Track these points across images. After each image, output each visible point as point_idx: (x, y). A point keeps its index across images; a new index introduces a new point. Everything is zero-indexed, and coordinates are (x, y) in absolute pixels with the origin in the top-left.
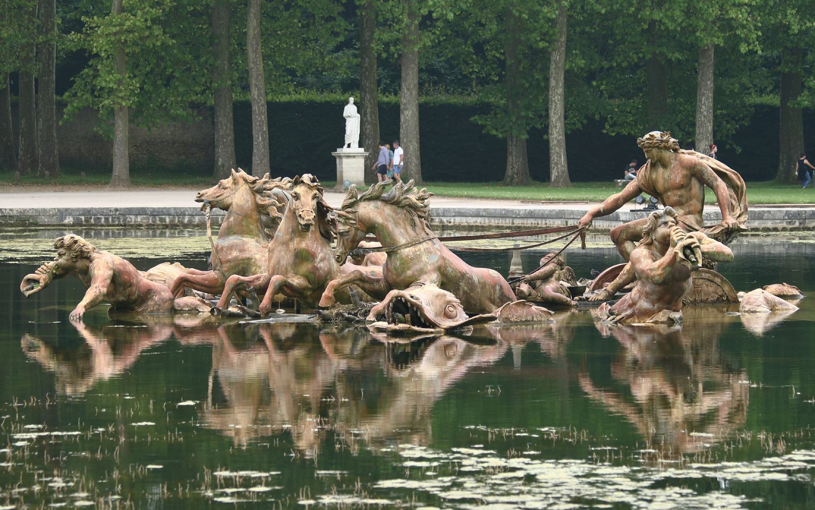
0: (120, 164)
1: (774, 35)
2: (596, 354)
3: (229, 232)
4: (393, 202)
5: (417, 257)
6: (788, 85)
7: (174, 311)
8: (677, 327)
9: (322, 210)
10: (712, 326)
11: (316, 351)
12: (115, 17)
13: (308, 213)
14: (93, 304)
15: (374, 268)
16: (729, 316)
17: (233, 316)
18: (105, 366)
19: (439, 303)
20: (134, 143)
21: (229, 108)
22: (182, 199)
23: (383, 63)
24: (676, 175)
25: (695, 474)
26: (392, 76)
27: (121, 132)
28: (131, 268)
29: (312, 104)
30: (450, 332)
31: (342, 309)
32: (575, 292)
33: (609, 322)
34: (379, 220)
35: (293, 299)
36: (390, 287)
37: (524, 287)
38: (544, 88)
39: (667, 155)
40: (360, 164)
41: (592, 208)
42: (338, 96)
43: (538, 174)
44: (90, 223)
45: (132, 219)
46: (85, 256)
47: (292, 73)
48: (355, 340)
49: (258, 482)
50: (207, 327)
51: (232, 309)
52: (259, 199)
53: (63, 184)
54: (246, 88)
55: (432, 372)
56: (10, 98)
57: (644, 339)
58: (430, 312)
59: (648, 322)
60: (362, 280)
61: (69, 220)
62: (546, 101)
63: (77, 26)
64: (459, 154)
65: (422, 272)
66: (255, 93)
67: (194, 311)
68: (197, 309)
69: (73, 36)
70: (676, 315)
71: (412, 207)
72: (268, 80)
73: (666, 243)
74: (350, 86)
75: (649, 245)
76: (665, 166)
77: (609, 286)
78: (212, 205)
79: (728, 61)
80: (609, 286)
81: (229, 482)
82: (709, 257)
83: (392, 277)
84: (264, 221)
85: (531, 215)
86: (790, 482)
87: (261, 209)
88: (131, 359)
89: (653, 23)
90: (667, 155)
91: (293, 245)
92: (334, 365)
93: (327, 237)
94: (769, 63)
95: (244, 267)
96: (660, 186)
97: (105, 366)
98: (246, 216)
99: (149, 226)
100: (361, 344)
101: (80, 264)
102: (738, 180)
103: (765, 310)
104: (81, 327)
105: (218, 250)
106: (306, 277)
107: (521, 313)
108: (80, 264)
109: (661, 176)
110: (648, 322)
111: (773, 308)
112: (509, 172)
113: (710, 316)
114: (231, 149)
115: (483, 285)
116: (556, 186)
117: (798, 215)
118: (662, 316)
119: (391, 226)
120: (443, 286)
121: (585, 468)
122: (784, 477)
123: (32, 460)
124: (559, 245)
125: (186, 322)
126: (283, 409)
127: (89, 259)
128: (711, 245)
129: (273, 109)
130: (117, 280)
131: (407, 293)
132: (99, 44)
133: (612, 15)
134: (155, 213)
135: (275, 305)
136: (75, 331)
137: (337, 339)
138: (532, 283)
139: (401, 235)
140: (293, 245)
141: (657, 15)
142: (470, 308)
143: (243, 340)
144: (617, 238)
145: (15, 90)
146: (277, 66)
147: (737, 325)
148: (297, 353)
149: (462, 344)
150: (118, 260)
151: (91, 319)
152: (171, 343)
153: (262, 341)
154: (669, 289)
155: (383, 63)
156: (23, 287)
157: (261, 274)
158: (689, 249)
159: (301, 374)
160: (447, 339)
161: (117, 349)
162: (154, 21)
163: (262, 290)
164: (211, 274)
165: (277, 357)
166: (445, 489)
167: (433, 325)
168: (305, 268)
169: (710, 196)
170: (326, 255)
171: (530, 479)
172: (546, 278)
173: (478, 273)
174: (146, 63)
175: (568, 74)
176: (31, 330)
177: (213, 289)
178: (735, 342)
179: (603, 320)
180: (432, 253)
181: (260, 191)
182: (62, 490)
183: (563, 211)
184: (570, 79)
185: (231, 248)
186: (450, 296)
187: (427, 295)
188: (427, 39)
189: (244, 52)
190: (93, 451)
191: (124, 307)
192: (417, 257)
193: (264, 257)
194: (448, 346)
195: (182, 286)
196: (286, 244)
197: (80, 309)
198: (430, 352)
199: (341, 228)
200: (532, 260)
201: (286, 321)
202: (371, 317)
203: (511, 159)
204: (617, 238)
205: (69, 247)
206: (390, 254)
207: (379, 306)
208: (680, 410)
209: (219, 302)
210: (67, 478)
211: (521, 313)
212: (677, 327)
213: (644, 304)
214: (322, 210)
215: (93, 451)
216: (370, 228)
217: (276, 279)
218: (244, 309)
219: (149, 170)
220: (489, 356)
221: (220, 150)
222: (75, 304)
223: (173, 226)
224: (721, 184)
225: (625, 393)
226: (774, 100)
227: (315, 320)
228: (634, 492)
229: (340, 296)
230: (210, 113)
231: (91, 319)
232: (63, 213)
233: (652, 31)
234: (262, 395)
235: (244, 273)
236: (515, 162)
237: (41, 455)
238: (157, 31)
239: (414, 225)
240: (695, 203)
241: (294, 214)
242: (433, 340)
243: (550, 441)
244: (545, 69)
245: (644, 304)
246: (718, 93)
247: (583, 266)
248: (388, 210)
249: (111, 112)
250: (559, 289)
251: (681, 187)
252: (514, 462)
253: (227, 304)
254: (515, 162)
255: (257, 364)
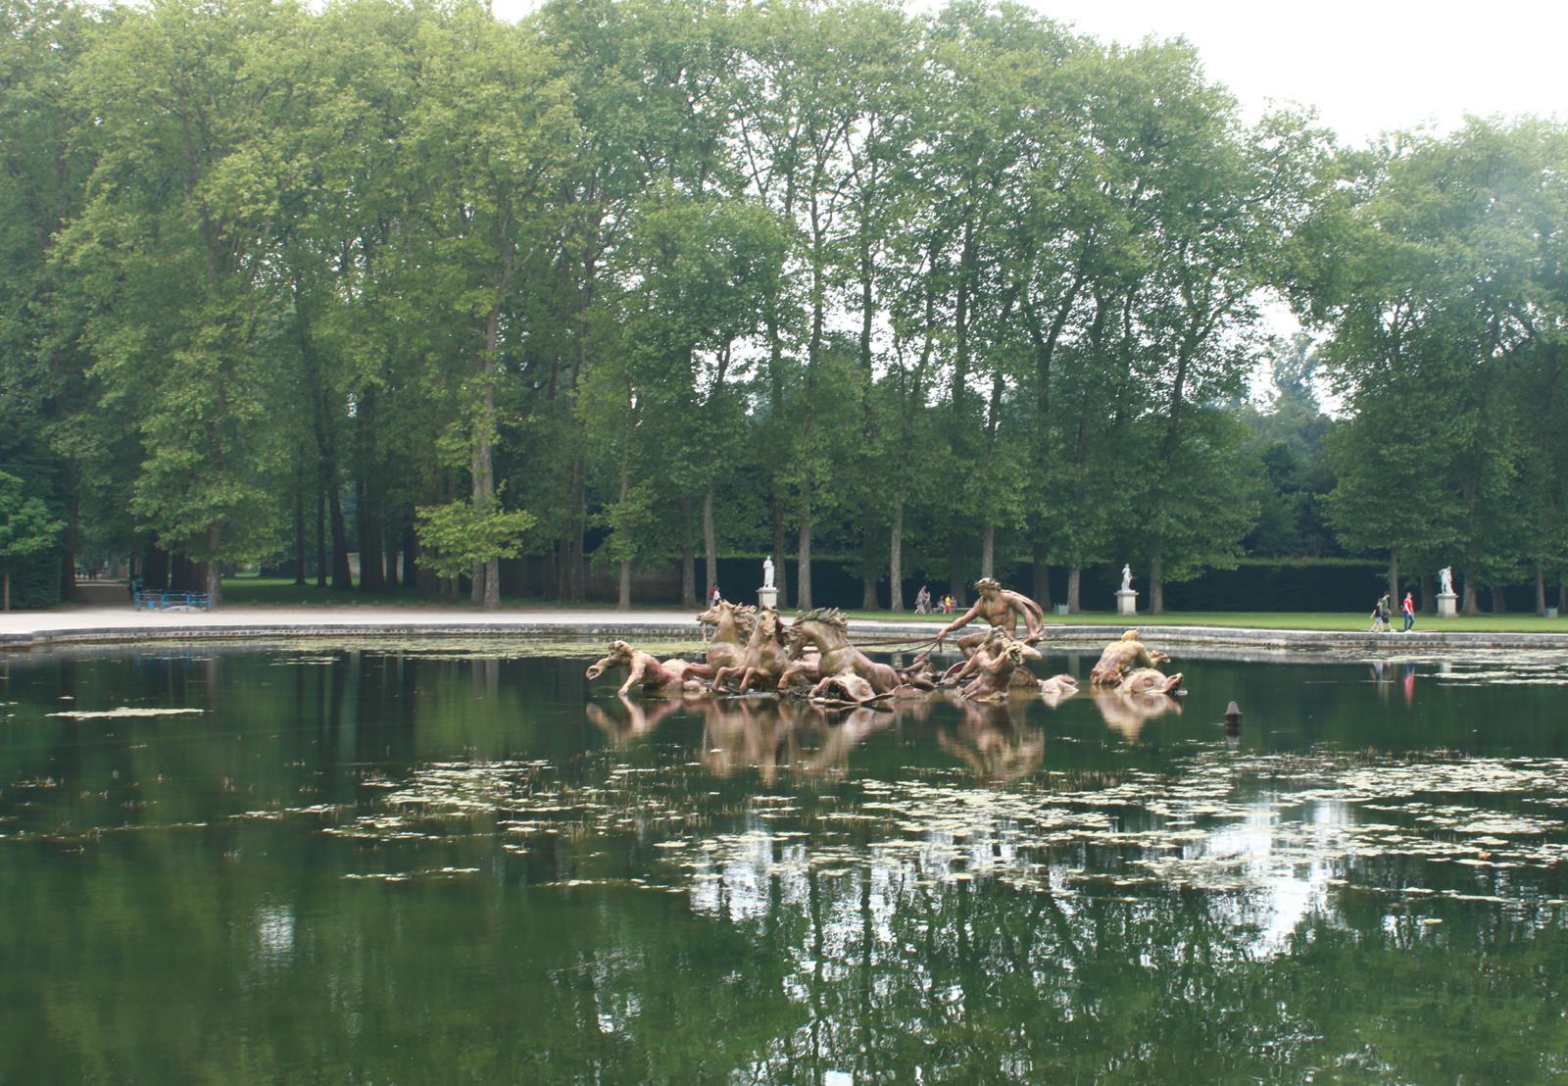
0: (624, 597)
1: (1033, 518)
2: (947, 716)
3: (718, 640)
4: (822, 621)
5: (840, 657)
6: (1040, 551)
7: (684, 690)
8: (1006, 702)
9: (779, 626)
10: (1023, 702)
11: (775, 715)
12: (622, 504)
13: (770, 629)
14: (633, 685)
15: (813, 661)
16: (1033, 696)
17: (722, 693)
18: (640, 723)
19: (857, 686)
20: (633, 584)
21: (692, 562)
22: (688, 620)
23: (788, 535)
24: (1000, 607)
25: (1066, 800)
26: (793, 543)
27: (625, 576)
28: (656, 662)
29: (743, 560)
30: (865, 704)
31: (792, 689)
32: (935, 679)
33: (963, 699)
34: (817, 633)
35: (759, 682)
36: (823, 675)
37: (904, 676)
38: (888, 552)
39: (994, 593)
40: (1453, 603)
41: (944, 627)
42: (758, 555)
43: (883, 604)
44: (629, 633)
45: (635, 631)
46: (627, 655)
47: (732, 540)
48: (801, 710)
49: (784, 804)
50: (705, 700)
51: (721, 689)
52: (737, 620)
53: (402, 606)
54: (703, 550)
55: (852, 729)
56: (554, 555)
57: (985, 709)
58: (852, 692)
59: (987, 699)
60: (805, 671)
61: (595, 631)
62: (890, 559)
63: (599, 510)
64: (840, 588)
65: (843, 666)
66: (708, 553)
67: (696, 690)
68: (698, 688)
69: (595, 516)
70: (1005, 695)
71: (837, 625)
72: (717, 544)
73: (999, 649)
74: (767, 549)
75: (988, 650)
76: (992, 600)
77: (957, 675)
78: (707, 622)
79: (1004, 535)
80: (957, 675)
81: (765, 804)
82: (1027, 658)
83: (824, 670)
84: (741, 635)
85: (886, 630)
86: (1127, 806)
87: (738, 626)
88: (657, 717)
89: (957, 511)
90: (994, 593)
91: (761, 649)
92: (786, 723)
93: (782, 643)
94: (1029, 537)
95: (727, 662)
96: (989, 612)
97: (640, 723)
98: (728, 630)
99: (647, 635)
100: (805, 712)
101: (624, 660)
102: (1039, 610)
103: (1058, 692)
104: (626, 700)
105: (711, 652)
106: (769, 669)
107: (907, 693)
108: (624, 660)
109: (990, 606)
110: (987, 699)
111: (1063, 690)
112: (866, 602)
113: (1021, 695)
114: (693, 587)
115: (881, 674)
116: (896, 612)
117: (1054, 631)
118: (996, 695)
119: (824, 637)
120: (857, 674)
121: (992, 795)
122: (1124, 802)
123: (630, 788)
124: (927, 649)
125: (690, 697)
126: (753, 751)
127: (631, 657)
128: (1027, 650)
129: (720, 562)
130: (649, 671)
131: (838, 679)
132: (613, 521)
133: (933, 505)
134: (650, 627)
135: (749, 686)
136: (621, 702)
137: (788, 709)
138: (908, 673)
139: (830, 642)
140: (761, 649)
141: (960, 507)
142: (877, 690)
143: (727, 708)
144: (962, 646)
145: (557, 549)
146: (722, 537)
147: (1040, 702)
148: (763, 716)
149: (871, 712)
150: (649, 657)
151: (633, 695)
152: (681, 711)
153: (740, 709)
154: (1001, 678)
155: (788, 535)
156: (588, 674)
157: (739, 666)
158: (1014, 653)
159: (765, 730)
160: (862, 709)
161: (648, 712)
162: (647, 507)
163: (741, 677)
164: (706, 666)
165: (749, 719)
166: (909, 809)
167: (854, 700)
168: (768, 663)
169: (1020, 620)
170: (781, 655)
171: (961, 803)
172: (918, 670)
173: (879, 667)
174: (637, 530)
175: (903, 542)
176: (595, 701)
177: (707, 676)
178: (1038, 710)
179: (957, 697)
180: (850, 654)
181: (737, 614)
182: (658, 809)
183: (925, 627)
184: (904, 545)
185: (719, 650)
186: (864, 682)
187: (849, 680)
188: (816, 520)
189: (702, 529)
190: (669, 782)
191: (652, 686)
192: (840, 657)
193: (741, 657)
194: (863, 713)
195: (688, 674)
196: (756, 648)
197: (625, 688)
198: (852, 717)
199: (792, 638)
200: (908, 659)
201: (755, 696)
202: (811, 695)
203: (867, 595)
204: (962, 646)
205: (618, 649)
206: (823, 655)
207: (816, 687)
208: (1007, 755)
209: (714, 684)
210: (660, 801)
211: (907, 693)
212: (1006, 702)
213: (985, 687)
214: (779, 626)
215: (669, 782)
216: (810, 638)
217: (750, 670)
218: (727, 688)
219: (643, 600)
220: (884, 719)
221: (686, 588)
222: (622, 685)
223: (661, 636)
224: (1027, 612)
225: (973, 747)
226: (1029, 559)
227: (775, 696)
228: (1032, 812)
229: (791, 681)
230: (680, 564)
231: (633, 695)
232: (591, 627)
233: (957, 517)
234: (739, 743)
235: (727, 665)
236: (869, 596)
237: (636, 784)
238: (649, 513)
239: (838, 636)
240: (1011, 624)
241: (761, 629)
242: (853, 710)
243: (959, 777)
244: (889, 540)
245: (985, 687)
246: (996, 555)
247: (938, 662)
248: (822, 627)
249: (618, 563)
250: (926, 677)
251: (1002, 613)
252: (943, 791)
253: (718, 685)
254: (869, 596)
255: (735, 723)
